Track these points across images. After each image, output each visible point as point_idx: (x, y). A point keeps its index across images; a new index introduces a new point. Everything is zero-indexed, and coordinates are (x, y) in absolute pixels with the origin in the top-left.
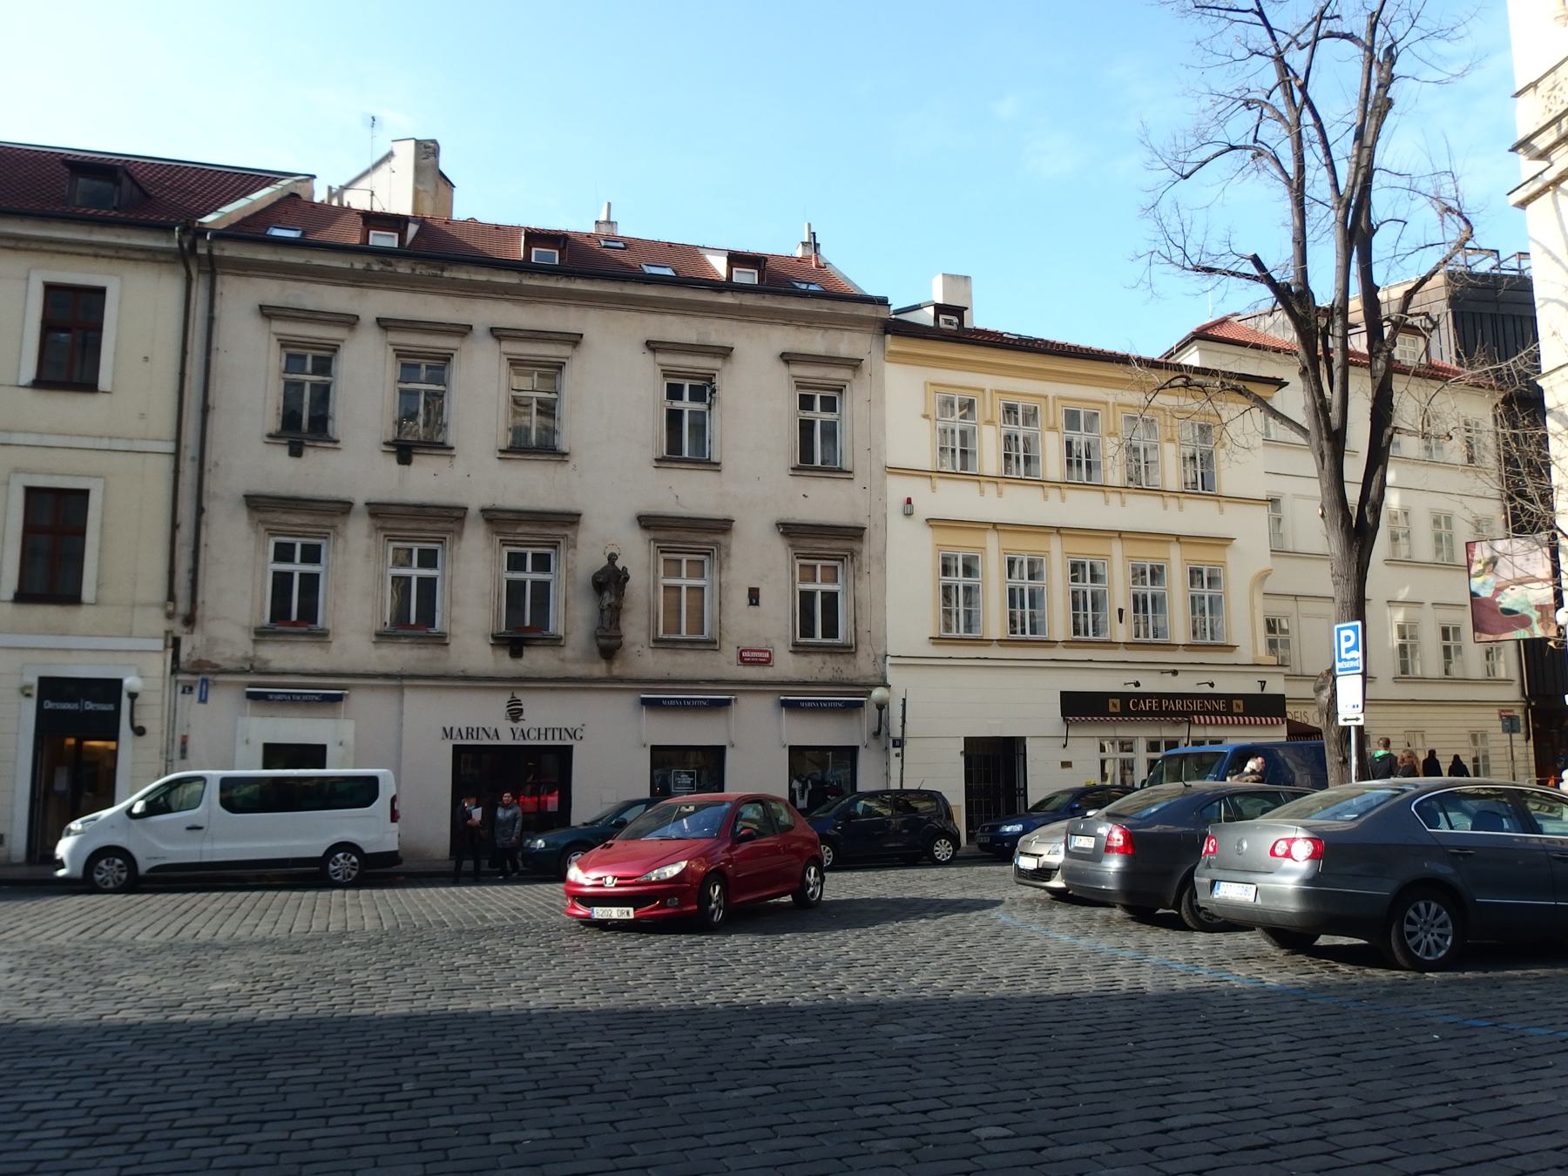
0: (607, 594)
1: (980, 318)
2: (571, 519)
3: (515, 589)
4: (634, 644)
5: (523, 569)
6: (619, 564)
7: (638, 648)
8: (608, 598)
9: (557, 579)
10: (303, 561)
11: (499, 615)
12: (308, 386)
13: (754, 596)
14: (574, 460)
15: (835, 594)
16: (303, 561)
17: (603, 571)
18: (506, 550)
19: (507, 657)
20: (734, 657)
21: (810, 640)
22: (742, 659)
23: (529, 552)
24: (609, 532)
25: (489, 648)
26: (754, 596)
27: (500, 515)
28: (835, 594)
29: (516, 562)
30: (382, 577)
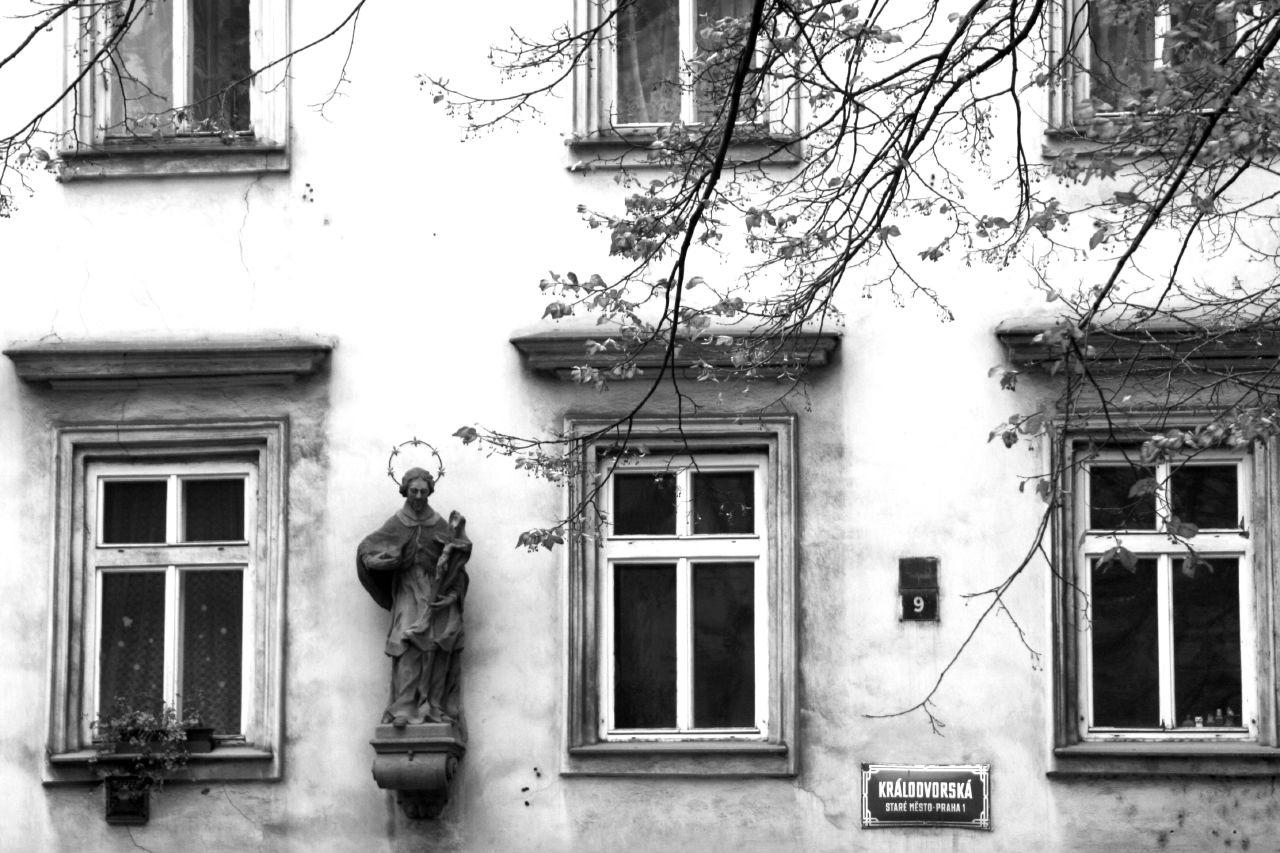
0: (404, 606)
1: (1103, 285)
2: (304, 369)
3: (131, 601)
4: (508, 767)
5: (155, 532)
6: (441, 503)
7: (524, 778)
8: (412, 618)
9: (254, 559)
10: (667, 571)
11: (75, 690)
12: (1167, 710)
13: (920, 591)
14: (304, 167)
15: (1227, 566)
16: (667, 571)
17: (389, 533)
18: (97, 478)
19: (99, 824)
20: (852, 797)
21: (711, 464)
22: (876, 804)
23: (174, 478)
24: (424, 399)
25: (41, 800)
26: (920, 591)
27: (67, 369)
28: (1227, 566)
29: (132, 512)
30: (75, 576)
